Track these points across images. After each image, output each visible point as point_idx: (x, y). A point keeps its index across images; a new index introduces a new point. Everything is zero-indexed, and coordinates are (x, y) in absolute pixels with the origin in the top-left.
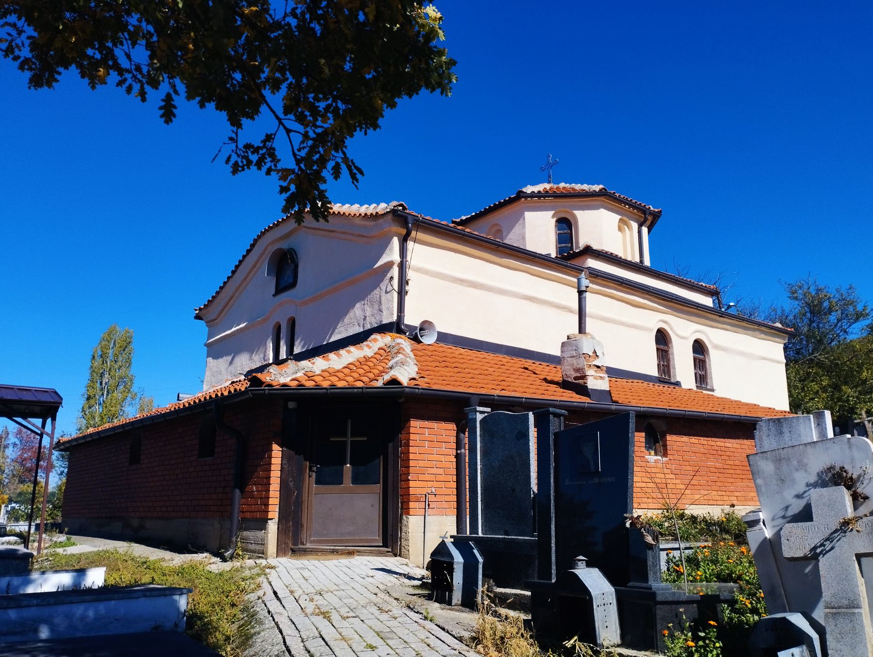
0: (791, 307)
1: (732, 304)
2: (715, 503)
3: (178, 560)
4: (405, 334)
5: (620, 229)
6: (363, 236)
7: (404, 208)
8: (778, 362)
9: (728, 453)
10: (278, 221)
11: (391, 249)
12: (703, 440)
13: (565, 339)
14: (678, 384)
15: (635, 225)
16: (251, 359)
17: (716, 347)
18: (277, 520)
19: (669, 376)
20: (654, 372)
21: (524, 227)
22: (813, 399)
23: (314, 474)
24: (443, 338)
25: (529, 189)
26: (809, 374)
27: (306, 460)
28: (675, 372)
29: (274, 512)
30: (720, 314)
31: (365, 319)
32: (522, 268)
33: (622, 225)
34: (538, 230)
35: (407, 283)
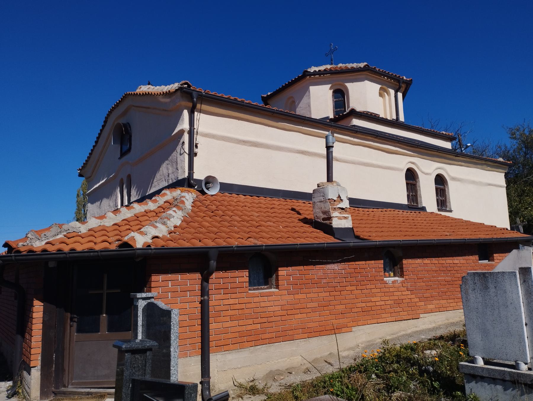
0: (511, 144)
1: (469, 145)
2: (445, 309)
4: (194, 187)
5: (381, 95)
6: (166, 110)
7: (189, 86)
8: (501, 186)
9: (456, 268)
10: (117, 103)
11: (183, 120)
12: (435, 260)
13: (316, 187)
14: (424, 209)
15: (392, 92)
16: (100, 207)
17: (454, 179)
18: (39, 367)
19: (417, 203)
20: (405, 202)
21: (309, 98)
22: (527, 208)
23: (75, 324)
24: (226, 188)
25: (312, 69)
26: (524, 191)
27: (67, 311)
28: (421, 200)
29: (36, 361)
30: (455, 155)
31: (168, 176)
32: (295, 129)
33: (381, 91)
34: (319, 101)
35: (197, 147)
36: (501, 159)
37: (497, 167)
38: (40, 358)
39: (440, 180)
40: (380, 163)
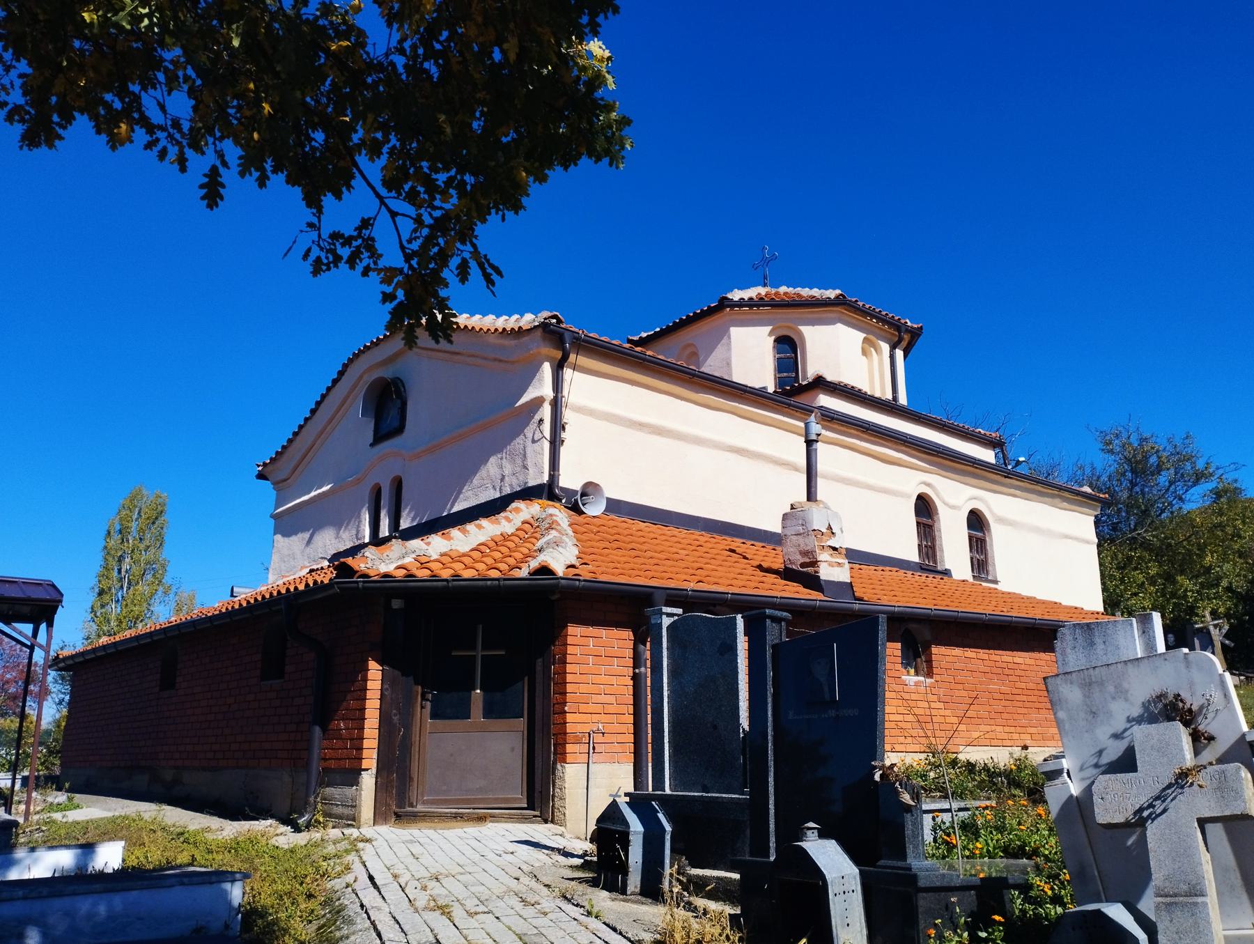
1: (1021, 459)
3: (228, 829)
4: (560, 500)
5: (864, 353)
6: (500, 361)
7: (559, 321)
8: (1088, 542)
10: (378, 339)
11: (541, 380)
12: (983, 653)
13: (788, 510)
14: (947, 573)
15: (885, 347)
16: (337, 537)
17: (1001, 520)
18: (374, 771)
19: (935, 562)
20: (913, 556)
21: (729, 349)
22: (1136, 594)
24: (614, 506)
25: (736, 295)
26: (1130, 559)
27: (417, 683)
28: (942, 557)
29: (370, 760)
30: (1004, 473)
31: (502, 480)
33: (866, 346)
34: (749, 353)
35: (564, 429)
36: (1087, 489)
37: (1080, 504)
38: (375, 756)
39: (976, 521)
40: (871, 481)
